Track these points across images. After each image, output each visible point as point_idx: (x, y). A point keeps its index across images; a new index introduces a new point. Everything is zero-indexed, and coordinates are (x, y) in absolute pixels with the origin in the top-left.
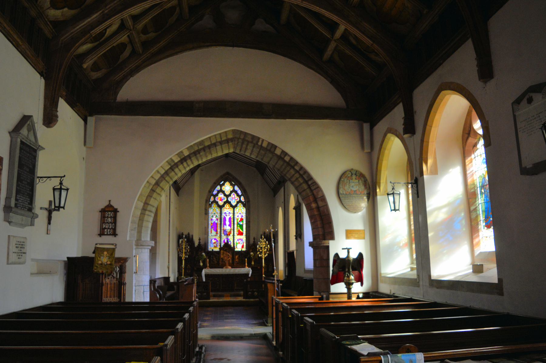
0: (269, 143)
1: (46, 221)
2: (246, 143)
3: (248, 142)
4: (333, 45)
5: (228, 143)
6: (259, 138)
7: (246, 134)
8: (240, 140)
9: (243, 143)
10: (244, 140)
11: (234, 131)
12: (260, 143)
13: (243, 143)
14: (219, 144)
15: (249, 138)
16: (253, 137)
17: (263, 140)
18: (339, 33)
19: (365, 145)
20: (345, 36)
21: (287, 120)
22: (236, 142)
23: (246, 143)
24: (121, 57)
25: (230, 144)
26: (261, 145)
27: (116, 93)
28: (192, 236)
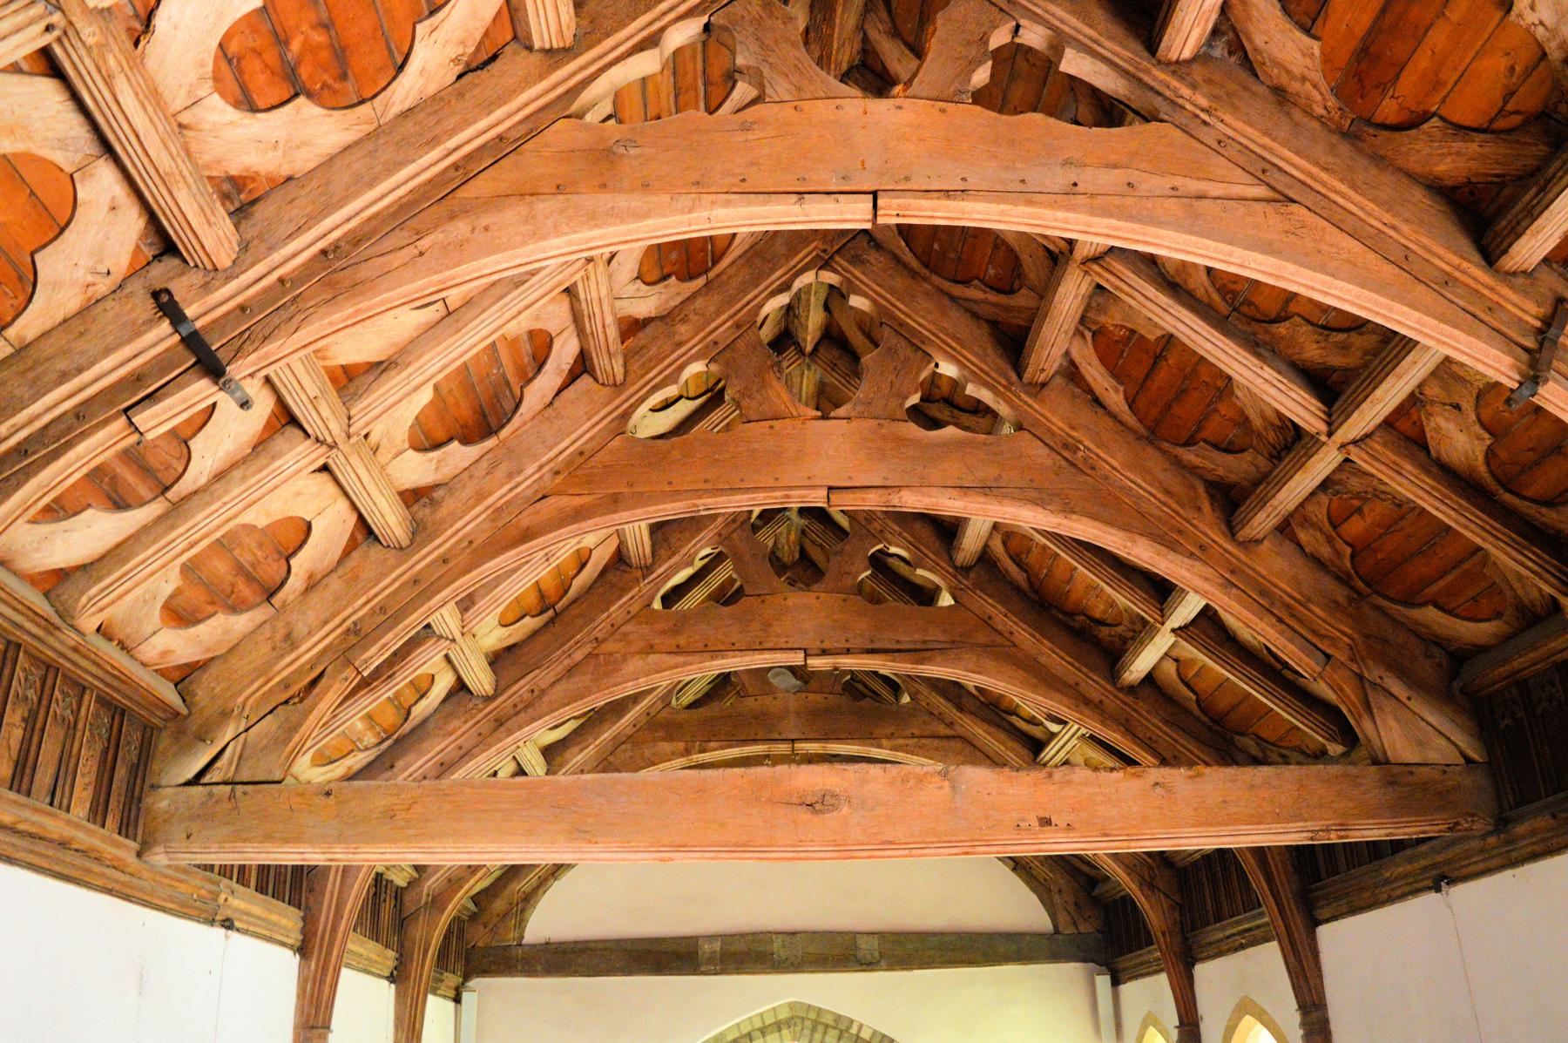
0: (875, 1032)
1: (1114, 1034)
2: (821, 1028)
3: (827, 1026)
4: (1323, 464)
5: (780, 1030)
6: (852, 1021)
7: (820, 1011)
8: (808, 1024)
9: (814, 1030)
10: (815, 1023)
11: (791, 1005)
12: (854, 1030)
13: (814, 1030)
14: (758, 1034)
15: (829, 1020)
16: (838, 1018)
17: (861, 1026)
18: (1186, 610)
19: (1102, 1026)
20: (1208, 626)
21: (916, 972)
22: (798, 1028)
23: (821, 1028)
24: (48, 263)
25: (785, 1032)
26: (858, 1036)
27: (521, 924)
28: (1278, 413)
